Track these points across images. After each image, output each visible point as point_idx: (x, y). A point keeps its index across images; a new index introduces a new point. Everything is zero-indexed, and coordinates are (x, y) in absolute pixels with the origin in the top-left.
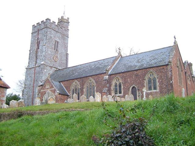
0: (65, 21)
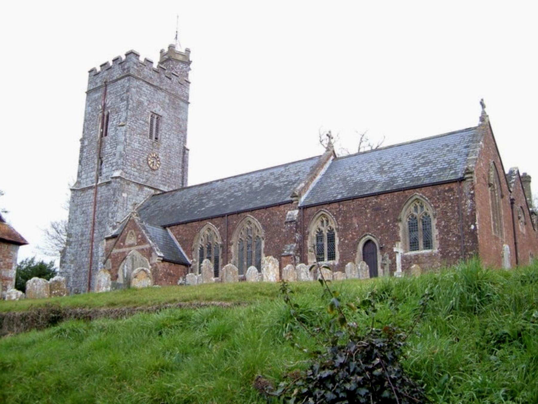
0: (180, 58)
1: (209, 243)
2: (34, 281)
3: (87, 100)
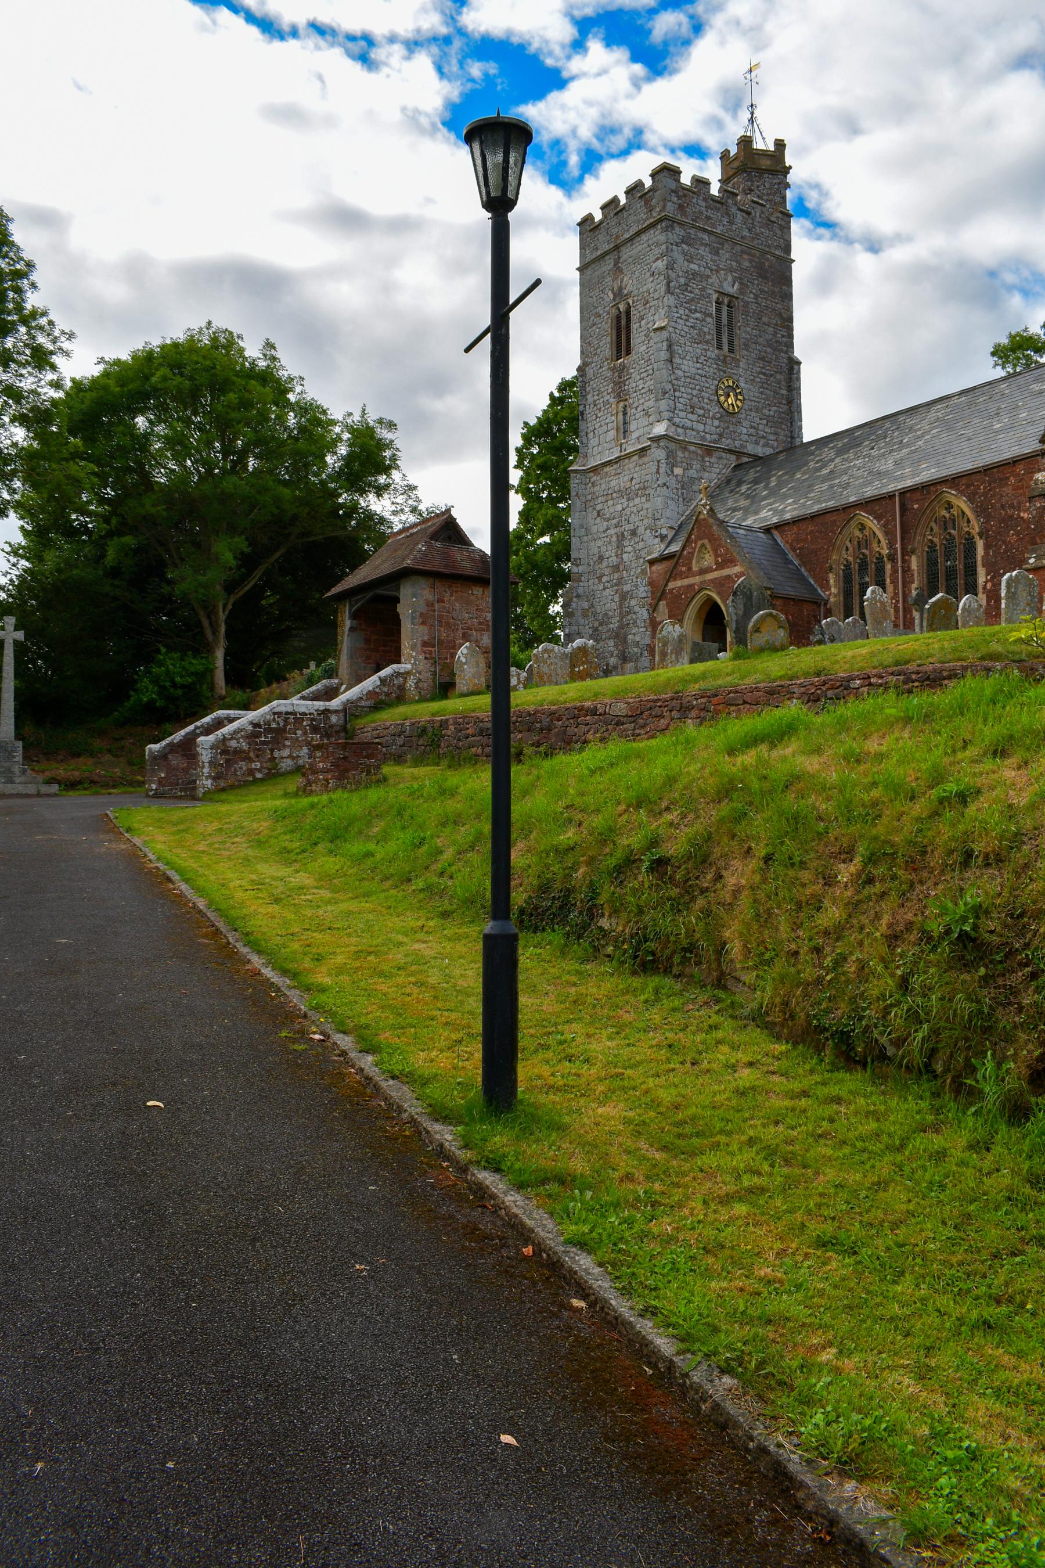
0: (765, 163)
1: (863, 554)
2: (545, 651)
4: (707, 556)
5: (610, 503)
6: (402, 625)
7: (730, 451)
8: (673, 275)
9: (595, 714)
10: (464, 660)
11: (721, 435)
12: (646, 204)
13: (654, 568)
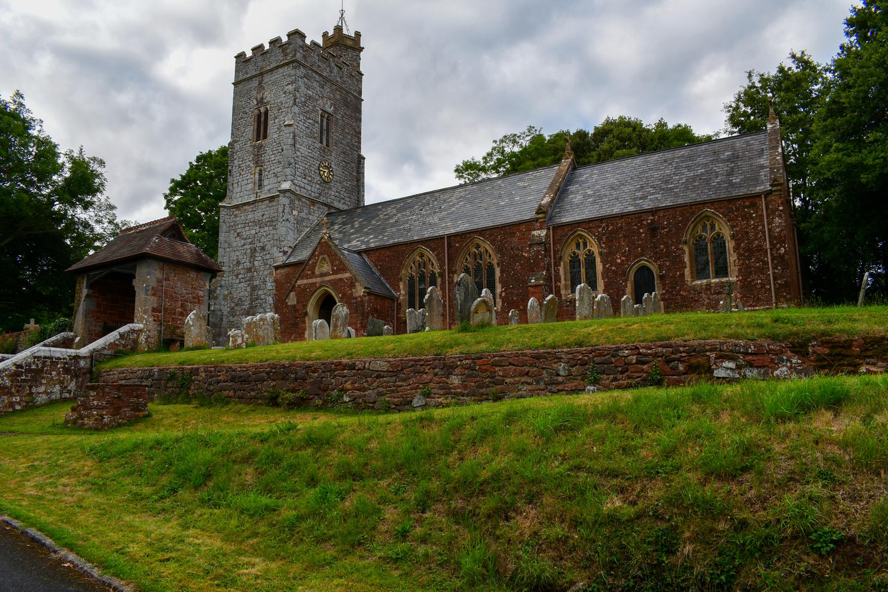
0: (350, 43)
3: (235, 93)
4: (326, 265)
5: (247, 228)
6: (137, 295)
7: (325, 205)
8: (298, 95)
9: (354, 369)
10: (191, 323)
11: (320, 194)
12: (283, 51)
13: (278, 271)
